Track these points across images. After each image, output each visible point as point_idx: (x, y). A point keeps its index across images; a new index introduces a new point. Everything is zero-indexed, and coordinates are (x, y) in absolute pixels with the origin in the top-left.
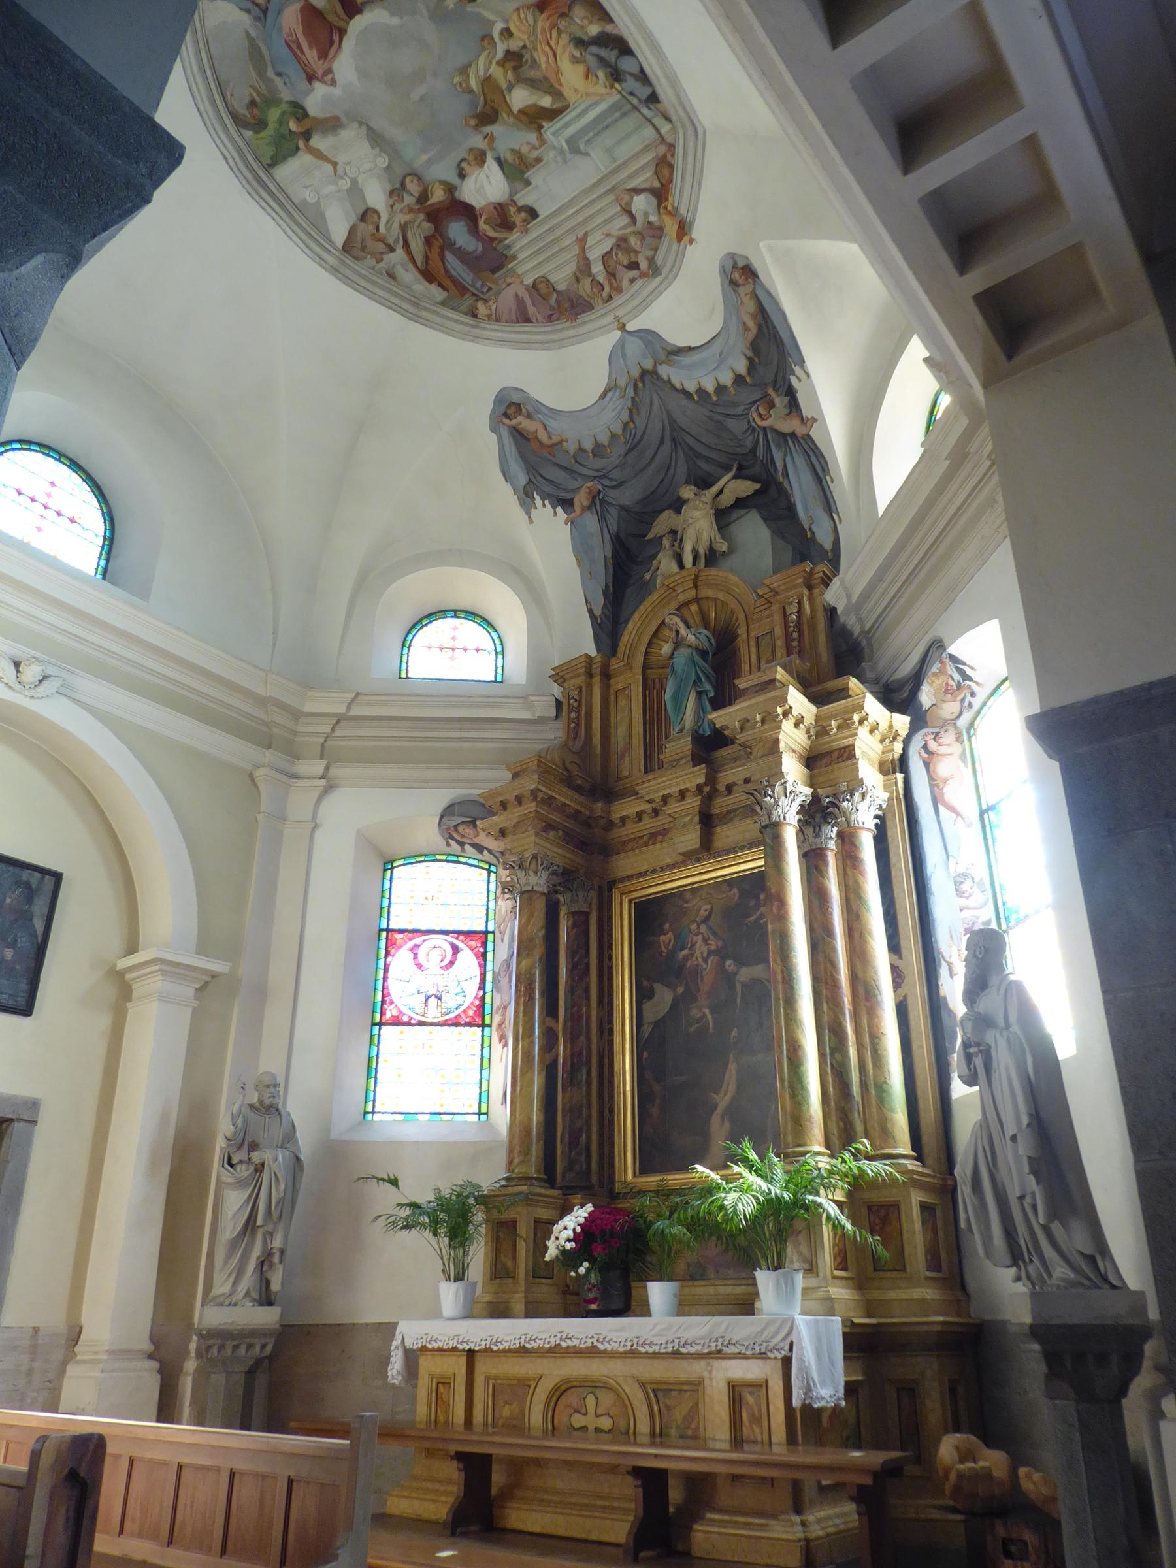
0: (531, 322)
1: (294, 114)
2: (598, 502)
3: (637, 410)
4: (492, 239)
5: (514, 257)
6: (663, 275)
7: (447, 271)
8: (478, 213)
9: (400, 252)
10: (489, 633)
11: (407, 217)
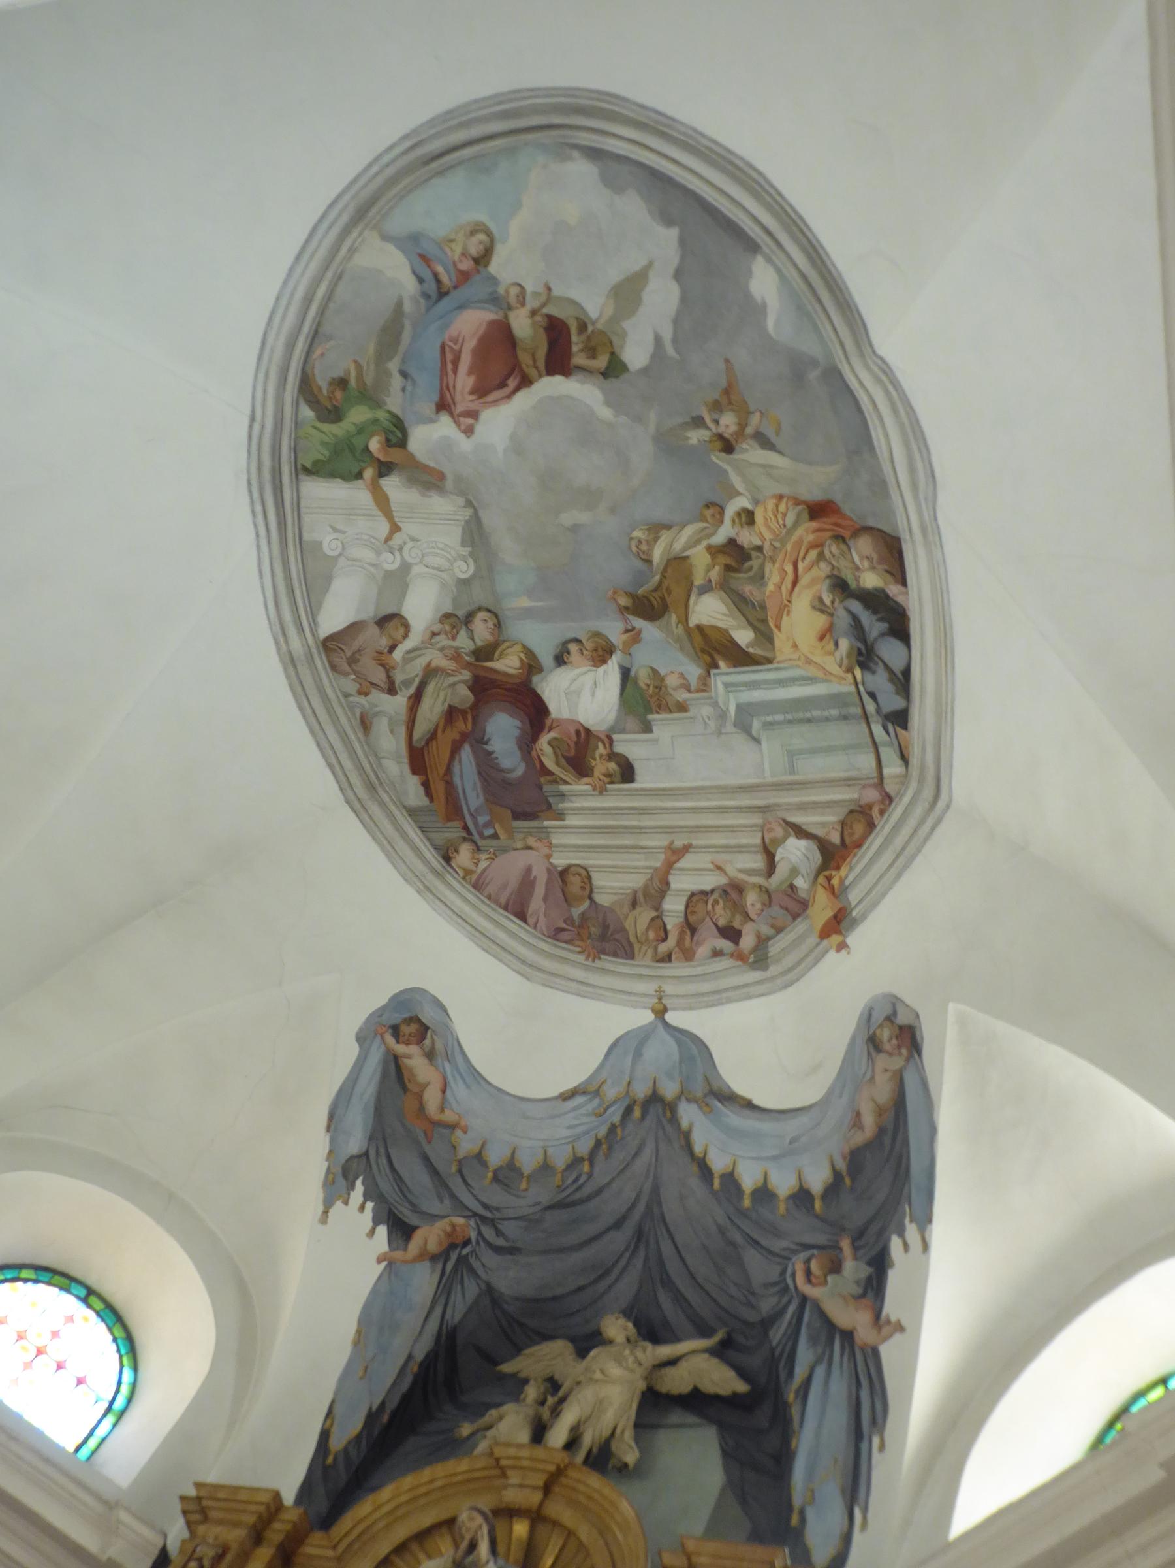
0: (525, 920)
1: (387, 431)
2: (454, 1257)
3: (610, 1148)
4: (545, 771)
5: (560, 816)
6: (768, 974)
7: (449, 770)
8: (548, 723)
9: (399, 703)
10: (122, 1367)
11: (441, 661)
